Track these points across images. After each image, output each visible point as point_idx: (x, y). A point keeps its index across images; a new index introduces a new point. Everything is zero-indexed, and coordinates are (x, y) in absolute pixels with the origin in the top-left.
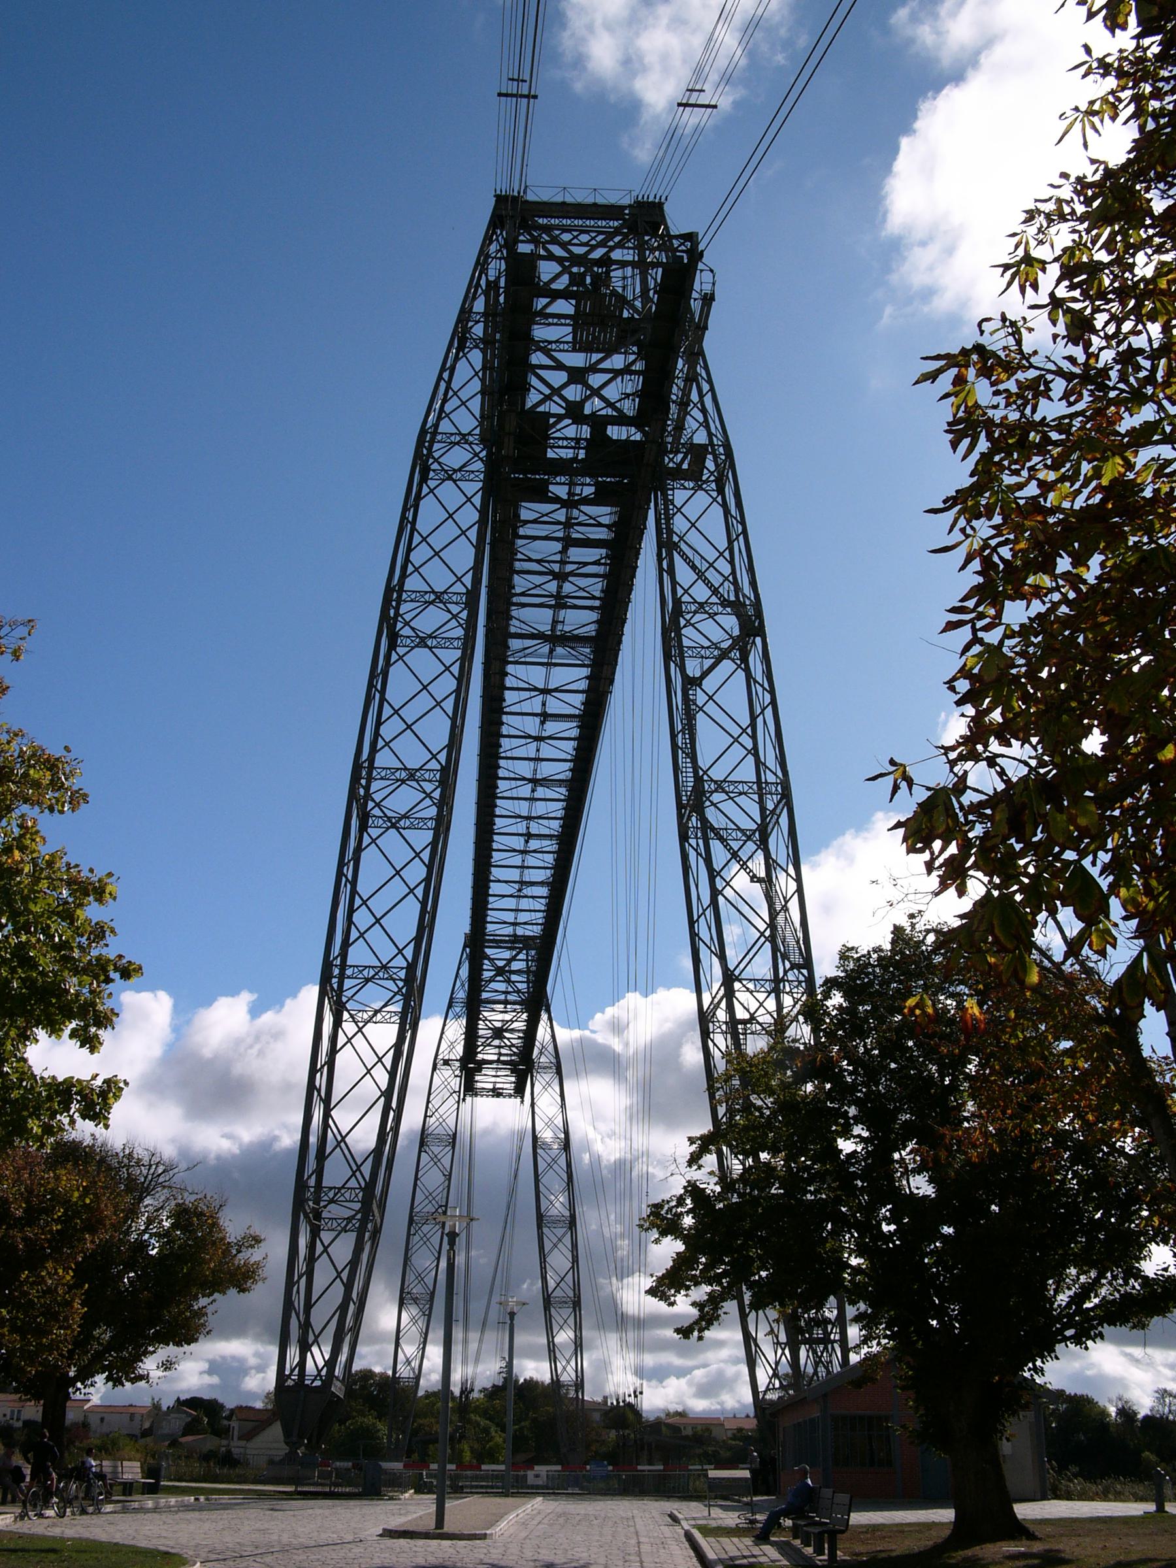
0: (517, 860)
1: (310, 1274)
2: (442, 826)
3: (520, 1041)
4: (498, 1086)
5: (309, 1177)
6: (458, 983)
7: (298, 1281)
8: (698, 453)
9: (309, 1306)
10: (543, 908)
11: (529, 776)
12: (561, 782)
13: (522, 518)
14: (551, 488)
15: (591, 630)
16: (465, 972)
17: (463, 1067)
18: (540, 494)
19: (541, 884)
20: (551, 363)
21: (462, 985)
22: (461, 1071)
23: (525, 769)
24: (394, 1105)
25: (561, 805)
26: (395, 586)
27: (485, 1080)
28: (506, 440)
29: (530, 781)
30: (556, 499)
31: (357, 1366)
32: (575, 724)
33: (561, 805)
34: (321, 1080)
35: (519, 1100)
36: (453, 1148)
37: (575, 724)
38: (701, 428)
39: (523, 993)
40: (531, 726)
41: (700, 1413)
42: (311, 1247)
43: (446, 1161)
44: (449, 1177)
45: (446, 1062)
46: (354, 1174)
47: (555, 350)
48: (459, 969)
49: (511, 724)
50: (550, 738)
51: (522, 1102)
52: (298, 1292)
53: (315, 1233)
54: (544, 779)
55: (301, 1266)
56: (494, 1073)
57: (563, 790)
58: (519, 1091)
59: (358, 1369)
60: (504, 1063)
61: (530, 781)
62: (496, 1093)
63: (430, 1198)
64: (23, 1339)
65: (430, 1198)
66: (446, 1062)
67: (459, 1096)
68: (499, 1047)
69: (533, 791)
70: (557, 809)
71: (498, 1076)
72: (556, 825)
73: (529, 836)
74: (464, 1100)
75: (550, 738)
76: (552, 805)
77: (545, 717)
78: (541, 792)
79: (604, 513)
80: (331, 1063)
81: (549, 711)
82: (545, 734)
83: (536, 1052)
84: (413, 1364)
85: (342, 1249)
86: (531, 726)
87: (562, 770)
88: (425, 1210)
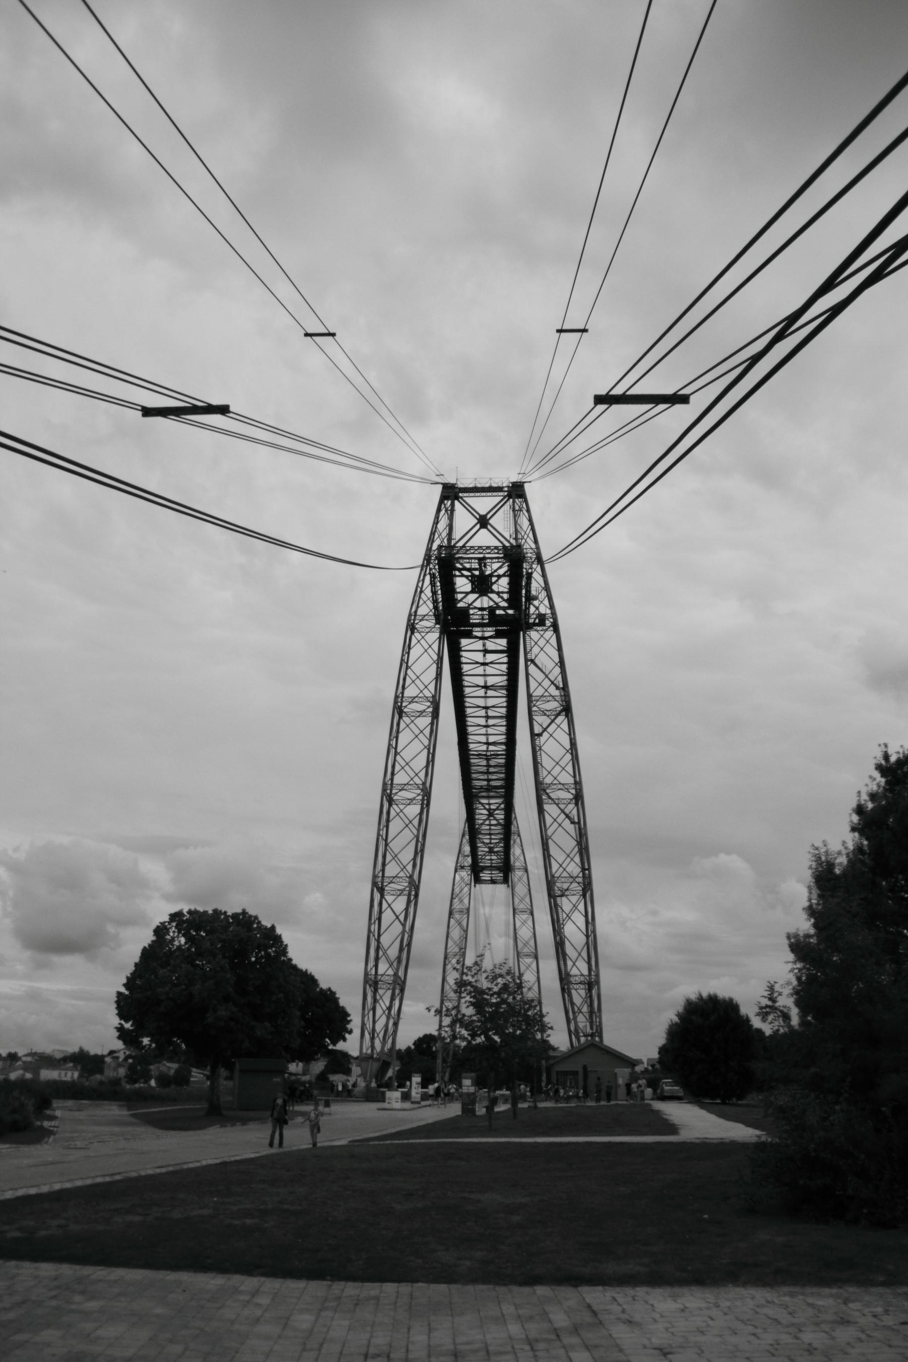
0: (483, 731)
1: (374, 1009)
2: (435, 715)
3: (501, 849)
4: (494, 878)
5: (371, 969)
7: (368, 1014)
8: (542, 619)
9: (374, 1022)
12: (502, 687)
13: (459, 599)
14: (474, 633)
15: (505, 683)
18: (469, 635)
20: (464, 595)
23: (480, 681)
24: (431, 755)
25: (504, 699)
26: (388, 781)
30: (476, 637)
32: (504, 720)
33: (504, 699)
35: (506, 885)
37: (504, 720)
38: (550, 836)
40: (479, 657)
43: (464, 923)
44: (466, 931)
46: (402, 870)
47: (465, 497)
49: (467, 680)
52: (368, 1018)
54: (492, 686)
56: (490, 872)
57: (505, 692)
61: (483, 687)
62: (493, 882)
68: (491, 843)
69: (486, 693)
70: (502, 701)
71: (493, 874)
72: (504, 711)
73: (487, 717)
76: (498, 700)
78: (490, 693)
79: (503, 643)
80: (380, 919)
82: (487, 661)
85: (400, 905)
87: (502, 680)
88: (453, 951)
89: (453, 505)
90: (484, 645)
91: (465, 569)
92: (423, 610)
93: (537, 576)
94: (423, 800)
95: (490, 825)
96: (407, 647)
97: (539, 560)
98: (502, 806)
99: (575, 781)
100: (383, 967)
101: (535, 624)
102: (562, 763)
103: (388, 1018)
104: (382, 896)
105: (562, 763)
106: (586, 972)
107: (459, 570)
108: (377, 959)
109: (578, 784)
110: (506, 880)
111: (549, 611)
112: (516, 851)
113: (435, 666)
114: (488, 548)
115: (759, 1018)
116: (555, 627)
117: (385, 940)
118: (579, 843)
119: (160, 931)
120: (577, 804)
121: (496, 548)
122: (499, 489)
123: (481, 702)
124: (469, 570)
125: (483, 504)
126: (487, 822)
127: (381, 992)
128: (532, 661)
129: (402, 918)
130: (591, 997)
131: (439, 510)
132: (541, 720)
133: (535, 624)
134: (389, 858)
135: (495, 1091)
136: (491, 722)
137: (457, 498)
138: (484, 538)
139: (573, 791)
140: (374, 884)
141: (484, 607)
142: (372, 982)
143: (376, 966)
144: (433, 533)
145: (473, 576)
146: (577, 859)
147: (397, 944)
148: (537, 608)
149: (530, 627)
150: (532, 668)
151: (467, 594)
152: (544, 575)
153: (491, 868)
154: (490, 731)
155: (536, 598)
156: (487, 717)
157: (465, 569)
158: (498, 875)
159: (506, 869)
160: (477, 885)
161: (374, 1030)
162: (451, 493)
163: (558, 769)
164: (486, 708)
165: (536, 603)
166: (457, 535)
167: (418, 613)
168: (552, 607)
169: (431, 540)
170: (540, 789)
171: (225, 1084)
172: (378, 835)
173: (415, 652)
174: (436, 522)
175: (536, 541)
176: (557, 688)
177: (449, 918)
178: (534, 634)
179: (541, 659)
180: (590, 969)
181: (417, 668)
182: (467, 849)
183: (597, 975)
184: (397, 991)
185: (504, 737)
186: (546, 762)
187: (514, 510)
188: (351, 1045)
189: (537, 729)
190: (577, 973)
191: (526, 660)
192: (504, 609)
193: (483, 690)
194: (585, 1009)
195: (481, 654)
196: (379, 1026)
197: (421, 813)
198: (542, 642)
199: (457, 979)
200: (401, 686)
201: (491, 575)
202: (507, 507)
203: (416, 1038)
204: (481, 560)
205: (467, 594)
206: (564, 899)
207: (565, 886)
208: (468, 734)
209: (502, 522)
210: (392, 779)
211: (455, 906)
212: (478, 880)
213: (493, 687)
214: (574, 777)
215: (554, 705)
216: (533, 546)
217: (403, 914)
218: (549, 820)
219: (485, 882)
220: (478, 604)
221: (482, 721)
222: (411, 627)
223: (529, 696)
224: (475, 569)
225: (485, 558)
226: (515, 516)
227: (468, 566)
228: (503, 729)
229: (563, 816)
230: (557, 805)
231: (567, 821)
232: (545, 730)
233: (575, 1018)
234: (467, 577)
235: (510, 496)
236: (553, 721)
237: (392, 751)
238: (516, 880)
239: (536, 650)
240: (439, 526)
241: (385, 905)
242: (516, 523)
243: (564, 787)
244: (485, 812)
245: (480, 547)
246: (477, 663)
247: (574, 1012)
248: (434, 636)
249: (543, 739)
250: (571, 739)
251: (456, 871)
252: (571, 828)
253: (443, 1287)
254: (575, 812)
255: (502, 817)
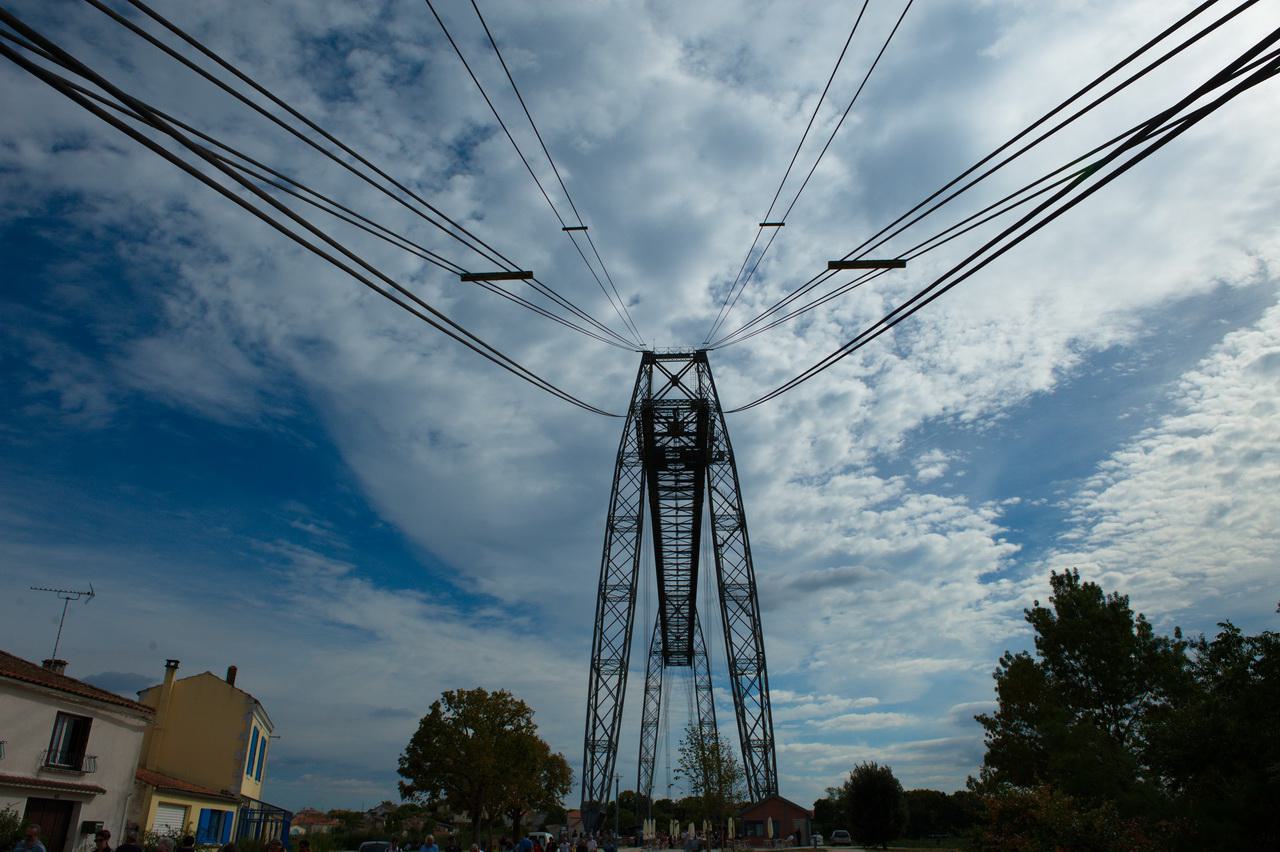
1: (592, 770)
2: (640, 531)
8: (721, 454)
9: (592, 780)
31: (621, 791)
34: (593, 701)
42: (592, 759)
44: (659, 705)
45: (655, 653)
53: (593, 753)
55: (589, 767)
62: (680, 664)
66: (655, 653)
70: (689, 519)
73: (678, 532)
76: (685, 560)
78: (680, 513)
80: (596, 695)
83: (695, 646)
89: (651, 368)
91: (662, 417)
92: (629, 449)
93: (718, 423)
94: (630, 598)
96: (617, 478)
97: (718, 409)
98: (687, 602)
99: (750, 581)
100: (600, 732)
101: (716, 459)
102: (740, 568)
103: (604, 776)
104: (599, 676)
105: (740, 568)
106: (762, 738)
107: (657, 418)
108: (594, 728)
109: (752, 584)
110: (690, 663)
111: (726, 449)
112: (697, 638)
113: (638, 492)
114: (681, 401)
115: (870, 368)
116: (732, 462)
117: (601, 712)
118: (754, 632)
119: (435, 707)
120: (751, 601)
121: (687, 401)
122: (687, 356)
123: (673, 520)
124: (665, 418)
125: (674, 367)
126: (675, 616)
127: (598, 755)
128: (715, 488)
129: (615, 693)
130: (767, 757)
131: (640, 372)
132: (722, 534)
133: (716, 459)
134: (603, 645)
135: (1004, 500)
136: (680, 535)
137: (655, 363)
138: (675, 394)
139: (748, 590)
140: (593, 665)
142: (590, 745)
143: (594, 734)
144: (636, 389)
145: (668, 422)
146: (753, 644)
147: (611, 715)
148: (718, 447)
149: (714, 461)
150: (715, 494)
152: (722, 421)
153: (677, 653)
154: (680, 542)
155: (717, 439)
156: (678, 532)
157: (662, 417)
158: (684, 659)
159: (690, 653)
160: (668, 668)
161: (592, 787)
162: (650, 358)
163: (736, 572)
164: (677, 524)
165: (717, 443)
166: (655, 390)
167: (626, 451)
168: (729, 444)
169: (635, 396)
170: (722, 588)
172: (596, 626)
173: (623, 482)
174: (639, 381)
175: (716, 395)
176: (734, 508)
178: (716, 468)
179: (721, 486)
180: (765, 734)
181: (626, 494)
182: (659, 638)
183: (772, 739)
184: (611, 754)
186: (726, 567)
187: (698, 372)
188: (572, 801)
189: (719, 541)
190: (755, 738)
191: (709, 486)
192: (692, 447)
193: (675, 511)
194: (763, 769)
196: (597, 783)
197: (629, 608)
198: (721, 473)
199: (564, 792)
200: (613, 508)
201: (682, 422)
202: (693, 369)
204: (675, 411)
206: (744, 676)
207: (744, 666)
209: (690, 380)
210: (606, 582)
212: (667, 663)
213: (683, 508)
214: (749, 578)
215: (732, 522)
216: (714, 399)
217: (616, 690)
218: (730, 614)
219: (672, 664)
220: (671, 444)
221: (674, 535)
222: (620, 463)
223: (713, 515)
224: (671, 417)
225: (678, 409)
226: (699, 376)
227: (664, 415)
228: (689, 541)
229: (741, 610)
230: (736, 601)
231: (744, 614)
232: (725, 542)
233: (755, 775)
234: (663, 423)
235: (695, 361)
236: (731, 535)
237: (606, 559)
238: (697, 662)
239: (717, 479)
240: (641, 384)
241: (601, 683)
242: (700, 382)
243: (741, 587)
244: (682, 611)
245: (675, 401)
247: (754, 771)
248: (637, 469)
249: (724, 549)
250: (745, 549)
251: (650, 655)
252: (747, 620)
254: (750, 607)
255: (667, 607)
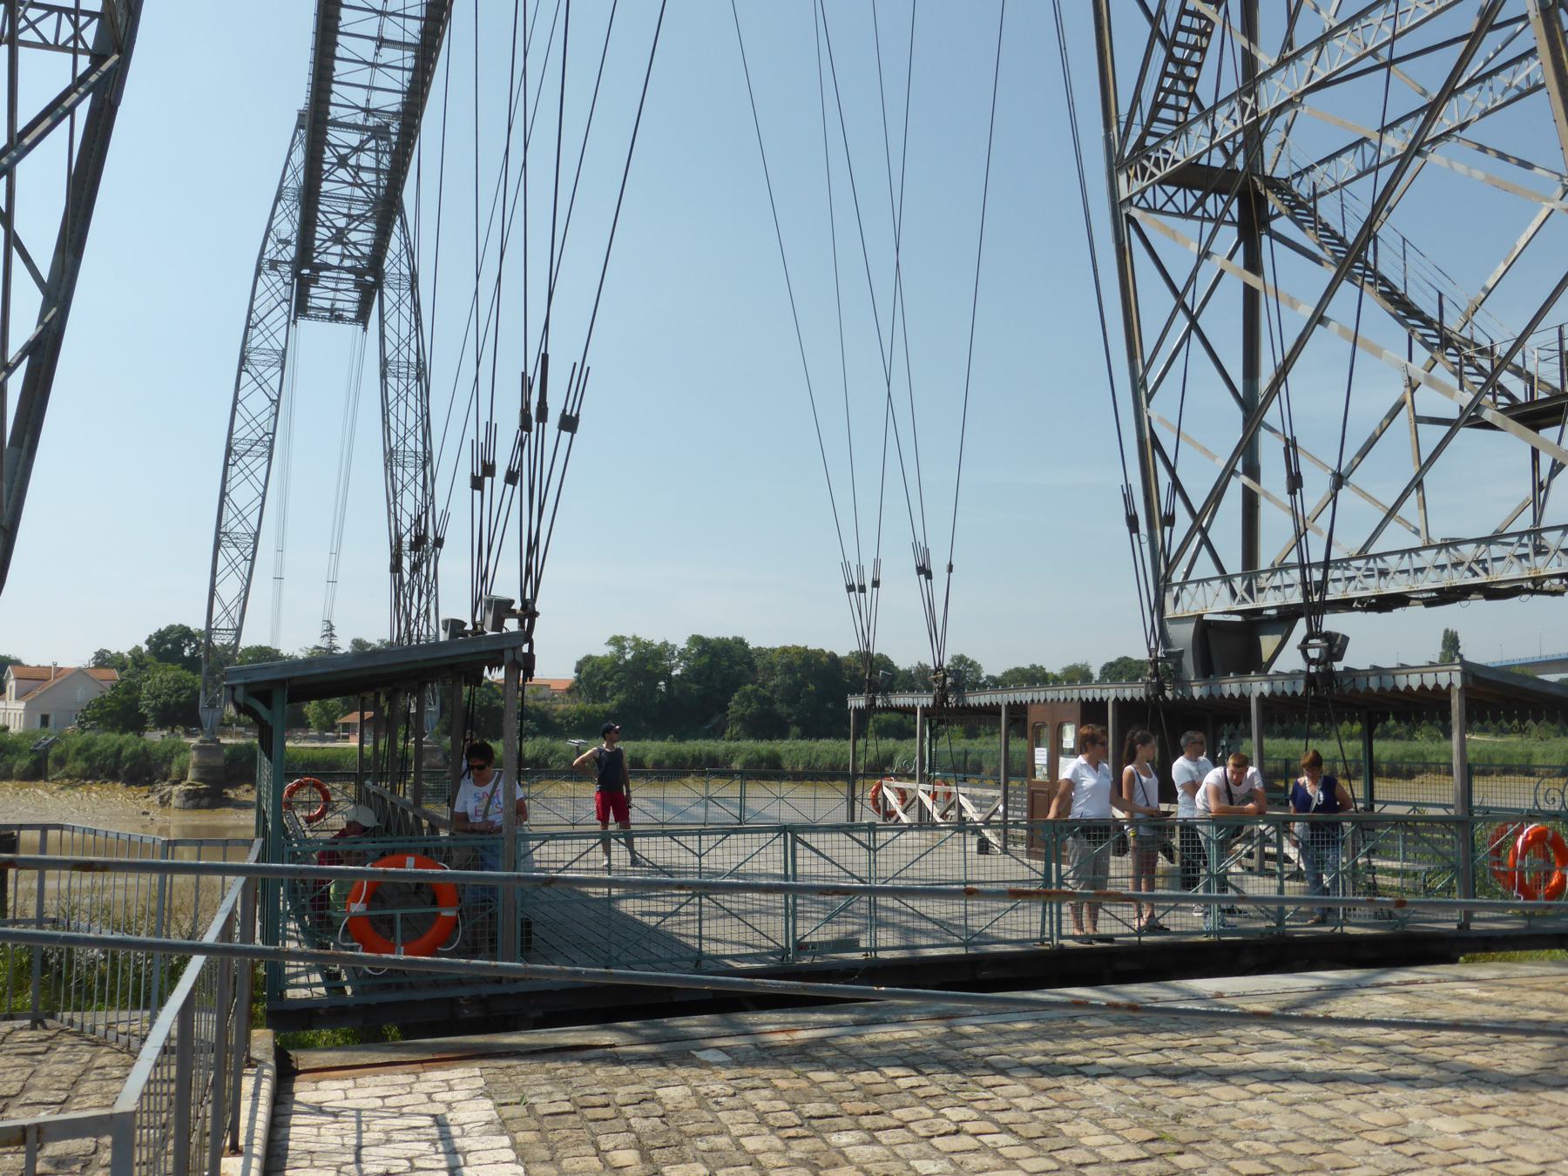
6: (289, 172)
10: (398, 87)
11: (363, 105)
16: (299, 157)
17: (296, 274)
19: (403, 45)
21: (295, 173)
22: (292, 279)
27: (320, 296)
28: (247, 1084)
29: (363, 110)
36: (283, 368)
39: (369, 187)
40: (367, 50)
41: (308, 662)
48: (290, 154)
49: (346, 46)
50: (385, 66)
51: (365, 329)
54: (376, 110)
56: (332, 285)
58: (362, 317)
59: (248, 646)
60: (349, 270)
61: (363, 110)
62: (335, 316)
63: (253, 424)
64: (1249, 838)
65: (253, 424)
66: (274, 264)
67: (290, 306)
71: (338, 290)
74: (295, 322)
75: (385, 66)
77: (381, 42)
81: (386, 37)
82: (380, 61)
84: (232, 613)
86: (367, 50)
90: (380, 27)
95: (359, 168)
141: (254, 823)
151: (325, 241)
154: (339, 296)
171: (141, 881)
177: (240, 371)
182: (287, 227)
185: (399, 98)
193: (362, 115)
195: (372, 45)
203: (153, 631)
205: (325, 241)
208: (334, 57)
211: (254, 344)
246: (365, 62)
253: (1386, 592)
